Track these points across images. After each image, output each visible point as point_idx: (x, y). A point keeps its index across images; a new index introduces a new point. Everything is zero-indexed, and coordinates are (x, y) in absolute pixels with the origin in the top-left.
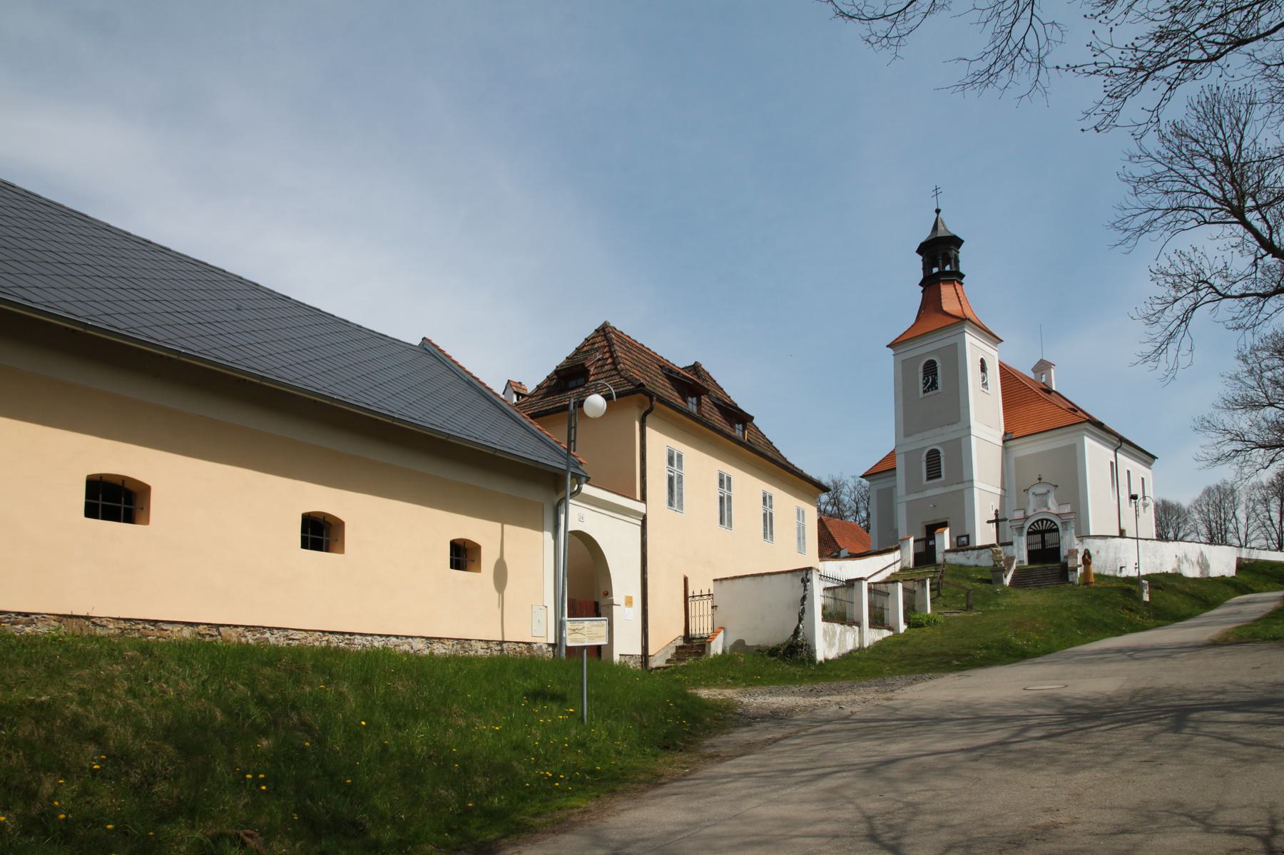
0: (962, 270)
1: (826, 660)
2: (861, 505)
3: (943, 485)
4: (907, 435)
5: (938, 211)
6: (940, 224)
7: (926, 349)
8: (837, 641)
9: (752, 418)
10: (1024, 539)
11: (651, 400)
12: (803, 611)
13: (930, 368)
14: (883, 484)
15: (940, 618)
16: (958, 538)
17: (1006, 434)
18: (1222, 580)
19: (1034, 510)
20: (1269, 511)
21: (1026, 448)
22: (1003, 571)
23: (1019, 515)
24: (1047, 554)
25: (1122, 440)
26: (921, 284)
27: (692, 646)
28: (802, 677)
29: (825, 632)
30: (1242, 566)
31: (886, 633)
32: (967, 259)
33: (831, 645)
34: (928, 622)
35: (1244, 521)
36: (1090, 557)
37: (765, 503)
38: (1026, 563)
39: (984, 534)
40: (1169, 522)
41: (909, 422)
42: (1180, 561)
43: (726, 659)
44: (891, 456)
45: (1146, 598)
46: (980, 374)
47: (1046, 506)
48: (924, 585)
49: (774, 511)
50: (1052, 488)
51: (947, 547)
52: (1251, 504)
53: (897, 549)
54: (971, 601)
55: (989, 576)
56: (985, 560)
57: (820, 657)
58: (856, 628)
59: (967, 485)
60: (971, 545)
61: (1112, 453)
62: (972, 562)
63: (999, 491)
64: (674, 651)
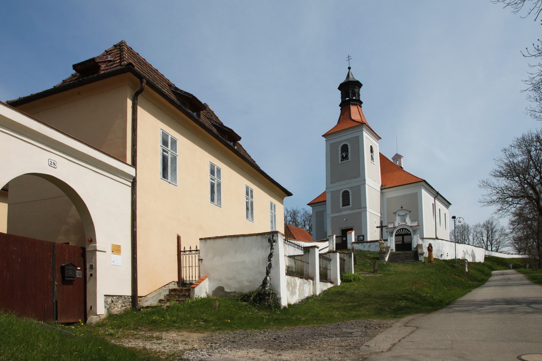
0: (361, 99)
1: (289, 305)
2: (306, 223)
3: (351, 209)
4: (332, 183)
5: (349, 68)
6: (350, 75)
7: (343, 138)
8: (297, 291)
9: (240, 138)
10: (393, 238)
11: (142, 82)
12: (270, 266)
13: (345, 149)
14: (319, 208)
15: (361, 277)
16: (358, 237)
17: (382, 186)
18: (480, 263)
19: (398, 222)
20: (482, 236)
21: (392, 194)
22: (385, 253)
23: (391, 226)
24: (406, 247)
25: (438, 193)
26: (340, 106)
27: (184, 288)
28: (268, 321)
29: (288, 284)
30: (487, 258)
31: (329, 285)
32: (364, 94)
33: (293, 293)
34: (354, 279)
35: (472, 240)
36: (432, 247)
37: (247, 194)
38: (394, 251)
39: (372, 233)
40: (460, 235)
41: (333, 174)
42: (465, 254)
43: (206, 302)
44: (324, 194)
45: (467, 270)
46: (370, 154)
47: (405, 221)
48: (350, 256)
49: (254, 200)
50: (408, 212)
51: (353, 240)
52: (475, 233)
53: (326, 241)
54: (376, 268)
55: (378, 256)
56: (374, 248)
57: (284, 303)
58: (311, 281)
59: (363, 209)
60: (365, 240)
61: (433, 199)
62: (366, 249)
63: (379, 215)
64: (167, 293)
